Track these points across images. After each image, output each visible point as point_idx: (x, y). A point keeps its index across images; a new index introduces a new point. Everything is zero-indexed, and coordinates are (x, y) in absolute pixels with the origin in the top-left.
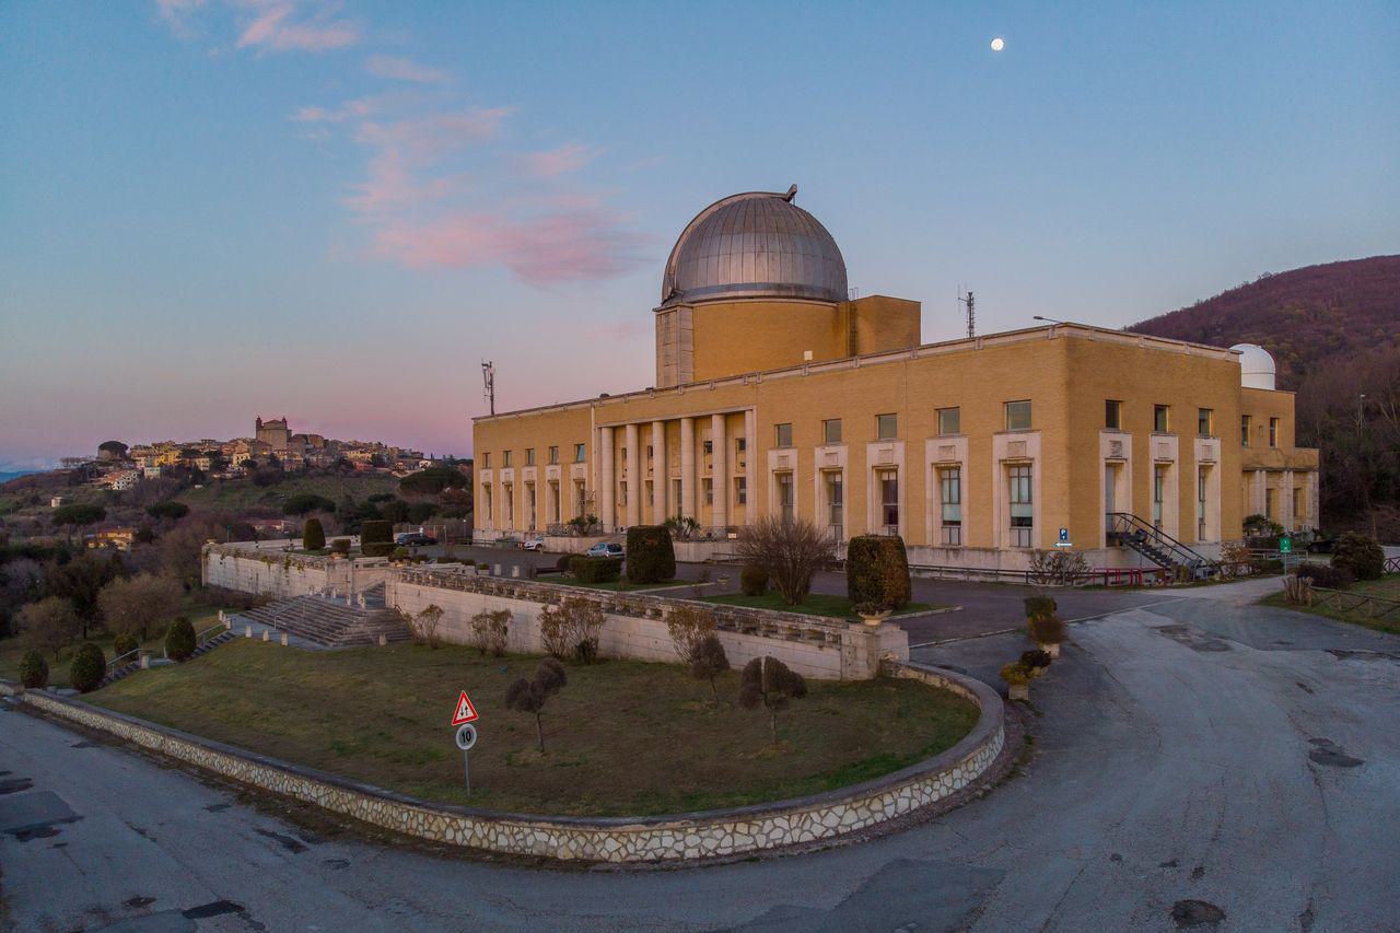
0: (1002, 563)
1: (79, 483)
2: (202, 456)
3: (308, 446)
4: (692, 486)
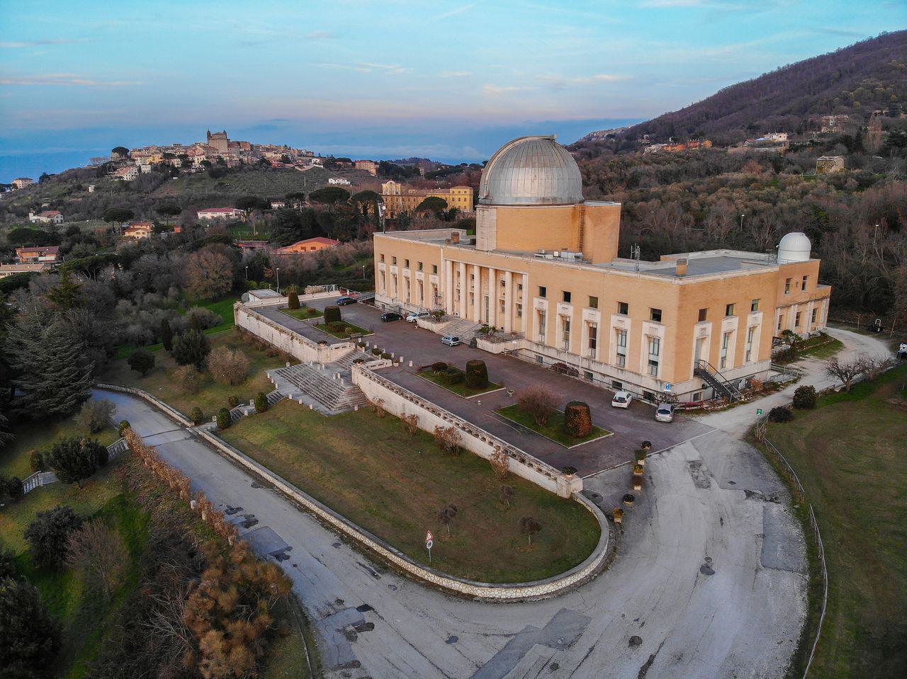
0: (643, 382)
1: (103, 176)
2: (176, 158)
3: (241, 150)
4: (494, 303)
